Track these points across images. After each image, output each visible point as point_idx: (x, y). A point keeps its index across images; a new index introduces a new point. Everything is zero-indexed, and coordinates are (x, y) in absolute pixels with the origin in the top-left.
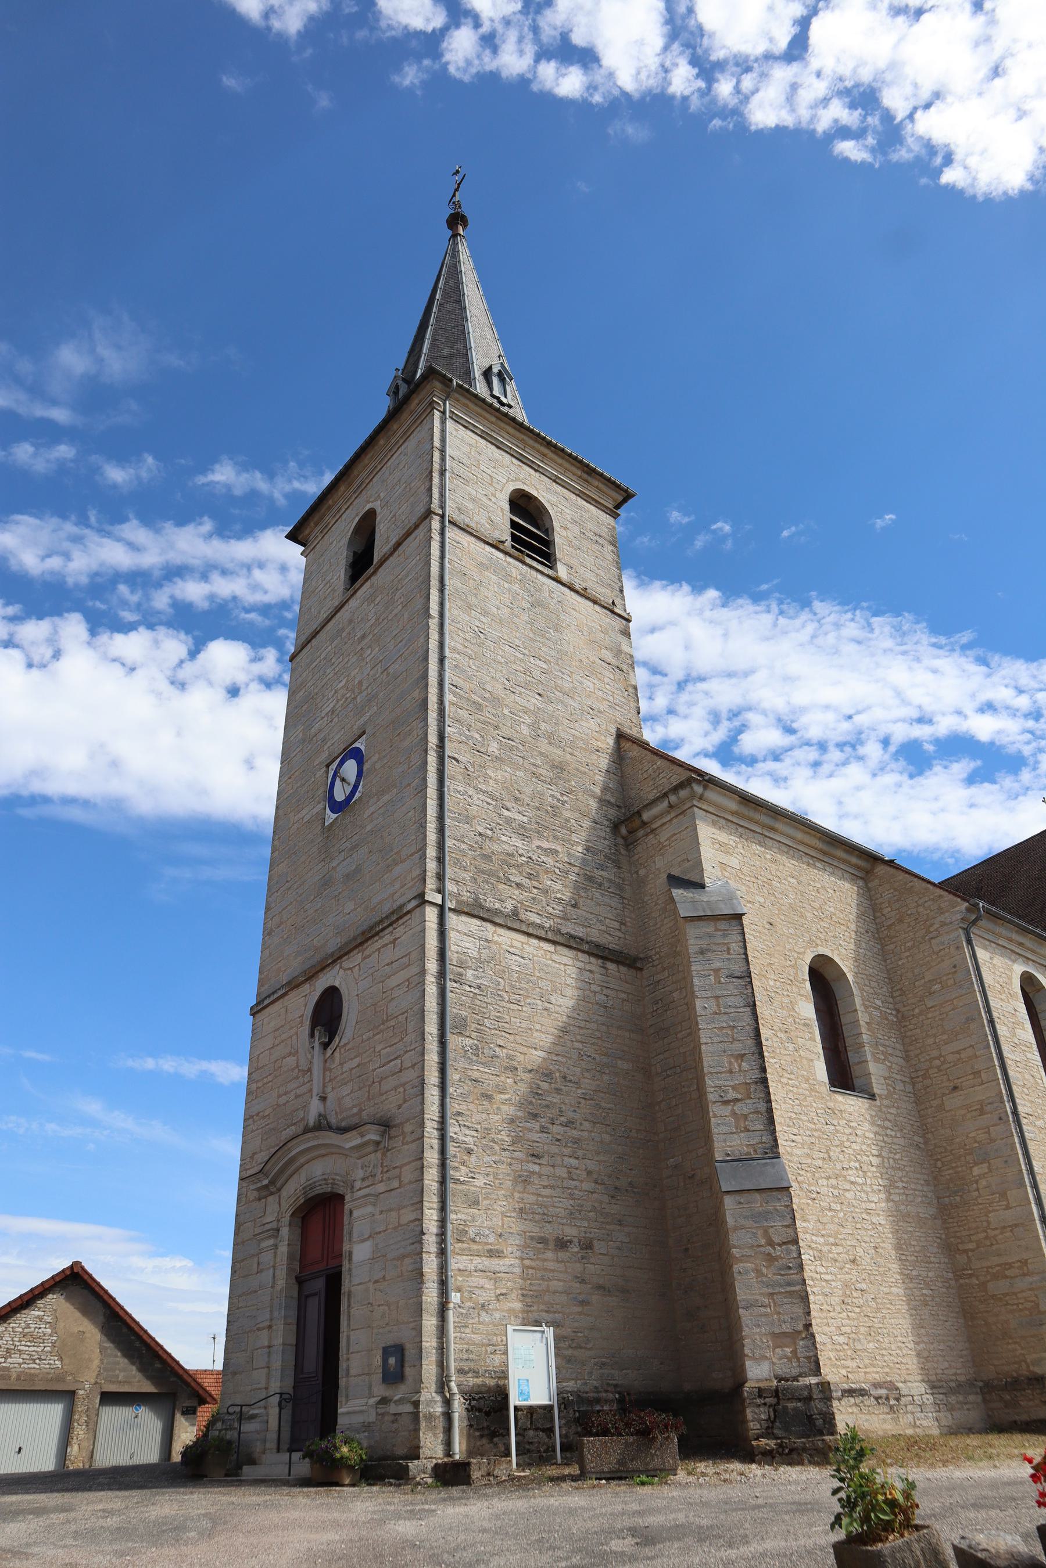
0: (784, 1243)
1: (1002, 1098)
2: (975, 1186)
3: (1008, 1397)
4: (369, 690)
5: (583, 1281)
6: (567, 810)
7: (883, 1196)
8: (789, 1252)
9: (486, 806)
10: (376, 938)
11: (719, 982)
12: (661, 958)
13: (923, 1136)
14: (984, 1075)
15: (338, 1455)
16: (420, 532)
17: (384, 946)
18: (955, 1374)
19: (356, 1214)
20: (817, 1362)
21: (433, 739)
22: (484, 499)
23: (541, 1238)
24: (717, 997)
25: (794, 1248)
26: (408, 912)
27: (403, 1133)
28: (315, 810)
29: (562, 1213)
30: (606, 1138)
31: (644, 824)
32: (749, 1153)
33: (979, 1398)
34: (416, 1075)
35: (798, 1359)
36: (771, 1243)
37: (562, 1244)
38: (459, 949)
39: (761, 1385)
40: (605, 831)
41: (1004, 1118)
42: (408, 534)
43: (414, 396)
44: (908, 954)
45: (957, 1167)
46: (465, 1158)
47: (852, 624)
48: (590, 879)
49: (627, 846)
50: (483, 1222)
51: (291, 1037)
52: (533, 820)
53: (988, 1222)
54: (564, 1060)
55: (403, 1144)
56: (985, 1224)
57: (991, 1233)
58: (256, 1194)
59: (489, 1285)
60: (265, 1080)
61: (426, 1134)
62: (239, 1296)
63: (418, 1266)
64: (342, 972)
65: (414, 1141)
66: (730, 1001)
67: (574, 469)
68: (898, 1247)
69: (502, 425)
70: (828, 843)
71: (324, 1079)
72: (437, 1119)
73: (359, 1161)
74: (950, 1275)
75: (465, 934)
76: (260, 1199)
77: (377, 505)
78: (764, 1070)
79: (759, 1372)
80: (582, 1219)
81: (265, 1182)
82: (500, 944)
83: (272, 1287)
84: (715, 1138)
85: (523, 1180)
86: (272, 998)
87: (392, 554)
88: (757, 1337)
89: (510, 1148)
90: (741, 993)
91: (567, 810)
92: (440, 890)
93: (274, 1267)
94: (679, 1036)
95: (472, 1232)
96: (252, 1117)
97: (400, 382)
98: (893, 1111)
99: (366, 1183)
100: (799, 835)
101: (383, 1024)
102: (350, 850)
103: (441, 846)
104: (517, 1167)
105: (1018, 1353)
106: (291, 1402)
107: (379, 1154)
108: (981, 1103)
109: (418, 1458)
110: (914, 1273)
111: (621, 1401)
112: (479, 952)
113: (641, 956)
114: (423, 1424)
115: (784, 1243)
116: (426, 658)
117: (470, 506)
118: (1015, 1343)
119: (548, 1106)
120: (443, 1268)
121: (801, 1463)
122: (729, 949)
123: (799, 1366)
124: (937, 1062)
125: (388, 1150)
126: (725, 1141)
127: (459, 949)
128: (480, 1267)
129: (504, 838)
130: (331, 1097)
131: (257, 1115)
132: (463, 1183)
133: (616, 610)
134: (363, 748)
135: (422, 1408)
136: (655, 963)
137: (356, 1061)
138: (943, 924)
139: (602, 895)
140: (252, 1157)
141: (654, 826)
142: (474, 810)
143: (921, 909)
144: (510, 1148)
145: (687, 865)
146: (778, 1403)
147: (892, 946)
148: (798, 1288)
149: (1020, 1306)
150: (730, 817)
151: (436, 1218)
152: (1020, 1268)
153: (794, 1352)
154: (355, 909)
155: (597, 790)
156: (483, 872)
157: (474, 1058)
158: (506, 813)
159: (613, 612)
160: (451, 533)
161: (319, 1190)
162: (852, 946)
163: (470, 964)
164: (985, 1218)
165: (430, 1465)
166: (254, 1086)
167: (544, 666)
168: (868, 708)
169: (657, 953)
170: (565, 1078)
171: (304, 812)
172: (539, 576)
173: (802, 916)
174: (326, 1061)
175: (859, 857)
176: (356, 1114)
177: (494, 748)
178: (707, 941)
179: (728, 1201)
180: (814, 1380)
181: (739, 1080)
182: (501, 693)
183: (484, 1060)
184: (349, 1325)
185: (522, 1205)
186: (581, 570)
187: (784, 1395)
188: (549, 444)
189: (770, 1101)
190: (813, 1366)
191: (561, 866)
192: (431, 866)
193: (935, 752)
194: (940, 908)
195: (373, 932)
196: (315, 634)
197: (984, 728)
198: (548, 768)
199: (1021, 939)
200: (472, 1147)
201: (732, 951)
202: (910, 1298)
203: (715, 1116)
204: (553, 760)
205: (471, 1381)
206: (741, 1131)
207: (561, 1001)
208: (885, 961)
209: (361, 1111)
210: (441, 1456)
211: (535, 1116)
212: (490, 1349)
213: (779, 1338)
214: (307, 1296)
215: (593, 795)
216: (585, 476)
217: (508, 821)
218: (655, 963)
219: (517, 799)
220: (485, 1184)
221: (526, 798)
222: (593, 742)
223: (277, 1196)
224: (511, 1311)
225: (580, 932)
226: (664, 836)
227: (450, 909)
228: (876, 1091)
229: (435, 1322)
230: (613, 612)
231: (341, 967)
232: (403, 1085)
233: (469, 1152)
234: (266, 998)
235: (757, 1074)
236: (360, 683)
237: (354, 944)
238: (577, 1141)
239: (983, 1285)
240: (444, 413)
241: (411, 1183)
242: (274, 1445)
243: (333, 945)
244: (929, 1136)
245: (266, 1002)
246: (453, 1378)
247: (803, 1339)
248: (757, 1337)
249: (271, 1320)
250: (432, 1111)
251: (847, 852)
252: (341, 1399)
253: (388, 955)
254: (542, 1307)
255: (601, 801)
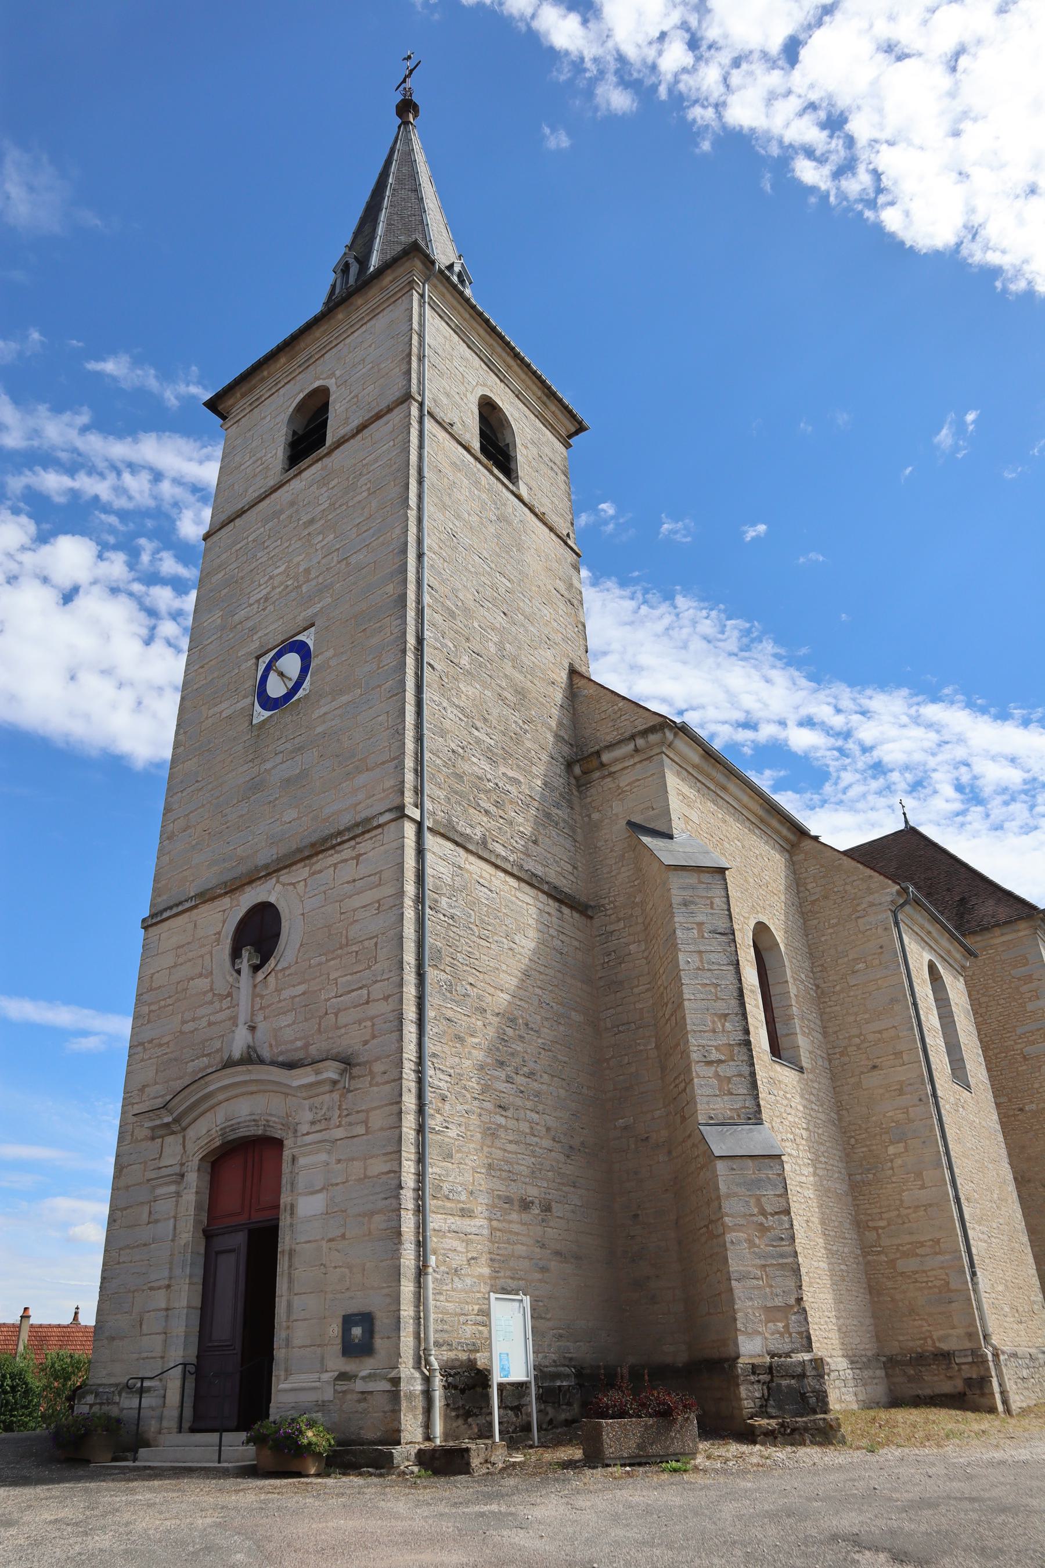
0: (776, 1213)
1: (923, 1079)
2: (889, 1164)
3: (912, 1372)
4: (320, 580)
5: (543, 1246)
6: (528, 739)
7: (811, 1170)
8: (781, 1223)
9: (459, 722)
10: (332, 852)
11: (703, 937)
12: (615, 907)
13: (838, 1113)
14: (905, 1057)
15: (305, 1441)
16: (396, 416)
17: (343, 861)
18: (865, 1349)
19: (302, 1161)
20: (809, 1338)
21: (411, 640)
22: (457, 397)
23: (507, 1197)
24: (700, 952)
25: (786, 1218)
26: (379, 826)
27: (371, 1072)
28: (240, 705)
29: (526, 1171)
30: (562, 1092)
31: (603, 765)
32: (732, 1118)
33: (880, 1373)
34: (390, 1008)
35: (790, 1335)
36: (763, 1213)
37: (525, 1205)
38: (435, 872)
39: (755, 1361)
40: (560, 769)
41: (924, 1099)
42: (378, 416)
43: (389, 271)
44: (830, 931)
45: (872, 1145)
46: (440, 1105)
47: (708, 622)
48: (548, 815)
49: (578, 786)
50: (455, 1178)
51: (202, 956)
52: (499, 745)
53: (901, 1201)
54: (526, 1006)
55: (371, 1085)
56: (898, 1202)
57: (904, 1212)
58: (149, 1133)
59: (460, 1247)
60: (163, 1003)
61: (404, 1076)
62: (121, 1249)
63: (394, 1224)
64: (279, 887)
65: (387, 1082)
66: (713, 957)
67: (534, 388)
68: (823, 1223)
69: (475, 325)
70: (767, 811)
71: (253, 1006)
72: (414, 1059)
73: (306, 1102)
74: (859, 1252)
75: (440, 857)
76: (153, 1139)
77: (331, 383)
78: (747, 1032)
79: (751, 1347)
80: (542, 1179)
81: (168, 1119)
82: (471, 873)
83: (173, 1240)
84: (698, 1099)
85: (491, 1133)
86: (175, 910)
87: (353, 436)
88: (750, 1310)
89: (481, 1097)
90: (725, 950)
91: (528, 739)
92: (419, 805)
93: (175, 1217)
94: (636, 990)
95: (446, 1187)
96: (142, 1044)
97: (351, 261)
98: (816, 1085)
99: (317, 1127)
100: (745, 799)
101: (341, 948)
102: (292, 752)
103: (419, 759)
104: (485, 1118)
105: (924, 1329)
106: (199, 1372)
107: (336, 1096)
108: (901, 1083)
109: (399, 1443)
110: (835, 1248)
111: (580, 1374)
112: (453, 879)
113: (592, 903)
114: (404, 1404)
115: (776, 1213)
116: (404, 551)
117: (445, 401)
118: (921, 1319)
119: (512, 1054)
120: (421, 1227)
121: (803, 1444)
122: (712, 903)
123: (791, 1342)
124: (857, 1041)
125: (349, 1091)
126: (708, 1103)
127: (435, 872)
128: (453, 1227)
129: (474, 759)
130: (262, 1026)
131: (151, 1041)
132: (438, 1133)
133: (569, 542)
134: (310, 643)
135: (403, 1386)
136: (608, 912)
137: (302, 988)
138: (872, 905)
139: (558, 835)
140: (142, 1089)
141: (613, 769)
142: (447, 724)
143: (848, 887)
144: (481, 1097)
145: (651, 813)
146: (772, 1381)
147: (815, 922)
148: (790, 1260)
149: (930, 1284)
150: (691, 770)
151: (413, 1171)
152: (931, 1247)
153: (787, 1327)
154: (299, 818)
155: (553, 724)
156: (456, 793)
157: (448, 995)
158: (476, 733)
159: (566, 543)
160: (429, 424)
161: (243, 1132)
162: (783, 918)
163: (444, 891)
164: (898, 1197)
165: (413, 1450)
166: (145, 1009)
167: (508, 584)
168: (702, 707)
169: (611, 902)
170: (527, 1025)
171: (223, 706)
172: (504, 490)
173: (746, 881)
174: (255, 986)
175: (789, 829)
176: (301, 1048)
177: (465, 661)
178: (690, 892)
179: (721, 1167)
180: (807, 1357)
181: (722, 1040)
182: (471, 604)
183: (457, 998)
184: (290, 1289)
185: (490, 1161)
186: (539, 494)
187: (778, 1372)
188: (517, 356)
189: (752, 1065)
190: (805, 1342)
191: (523, 798)
192: (409, 777)
193: (752, 756)
194: (869, 888)
195: (329, 845)
196: (241, 513)
197: (801, 739)
198: (512, 692)
199: (928, 926)
200: (447, 1093)
201: (715, 906)
202: (832, 1273)
203: (698, 1076)
204: (516, 685)
205: (447, 1355)
206: (725, 1094)
207: (524, 942)
208: (807, 936)
209: (306, 1046)
210: (420, 1440)
211: (501, 1064)
212: (462, 1319)
213: (772, 1313)
214: (218, 1253)
215: (550, 729)
216: (545, 398)
217: (478, 741)
218: (608, 912)
219: (485, 720)
220: (458, 1135)
221: (494, 721)
222: (550, 673)
223: (180, 1136)
224: (480, 1276)
225: (539, 871)
226: (624, 780)
227: (428, 828)
228: (804, 1065)
229: (412, 1289)
230: (566, 543)
231: (278, 882)
232: (372, 1018)
233: (444, 1099)
234: (165, 910)
235: (741, 1036)
236: (307, 571)
237: (299, 857)
238: (538, 1094)
239: (892, 1263)
240: (422, 296)
241: (382, 1129)
242: (174, 1424)
243: (265, 856)
244: (844, 1112)
245: (165, 915)
246: (433, 1352)
247: (795, 1313)
248: (750, 1310)
249: (170, 1278)
250: (410, 1051)
251: (780, 822)
252: (278, 1372)
253: (348, 871)
254: (508, 1273)
255: (557, 736)
